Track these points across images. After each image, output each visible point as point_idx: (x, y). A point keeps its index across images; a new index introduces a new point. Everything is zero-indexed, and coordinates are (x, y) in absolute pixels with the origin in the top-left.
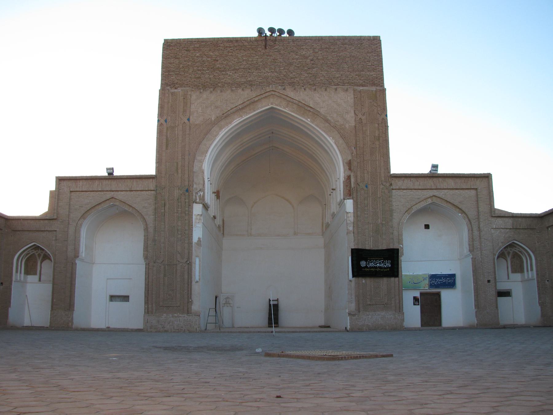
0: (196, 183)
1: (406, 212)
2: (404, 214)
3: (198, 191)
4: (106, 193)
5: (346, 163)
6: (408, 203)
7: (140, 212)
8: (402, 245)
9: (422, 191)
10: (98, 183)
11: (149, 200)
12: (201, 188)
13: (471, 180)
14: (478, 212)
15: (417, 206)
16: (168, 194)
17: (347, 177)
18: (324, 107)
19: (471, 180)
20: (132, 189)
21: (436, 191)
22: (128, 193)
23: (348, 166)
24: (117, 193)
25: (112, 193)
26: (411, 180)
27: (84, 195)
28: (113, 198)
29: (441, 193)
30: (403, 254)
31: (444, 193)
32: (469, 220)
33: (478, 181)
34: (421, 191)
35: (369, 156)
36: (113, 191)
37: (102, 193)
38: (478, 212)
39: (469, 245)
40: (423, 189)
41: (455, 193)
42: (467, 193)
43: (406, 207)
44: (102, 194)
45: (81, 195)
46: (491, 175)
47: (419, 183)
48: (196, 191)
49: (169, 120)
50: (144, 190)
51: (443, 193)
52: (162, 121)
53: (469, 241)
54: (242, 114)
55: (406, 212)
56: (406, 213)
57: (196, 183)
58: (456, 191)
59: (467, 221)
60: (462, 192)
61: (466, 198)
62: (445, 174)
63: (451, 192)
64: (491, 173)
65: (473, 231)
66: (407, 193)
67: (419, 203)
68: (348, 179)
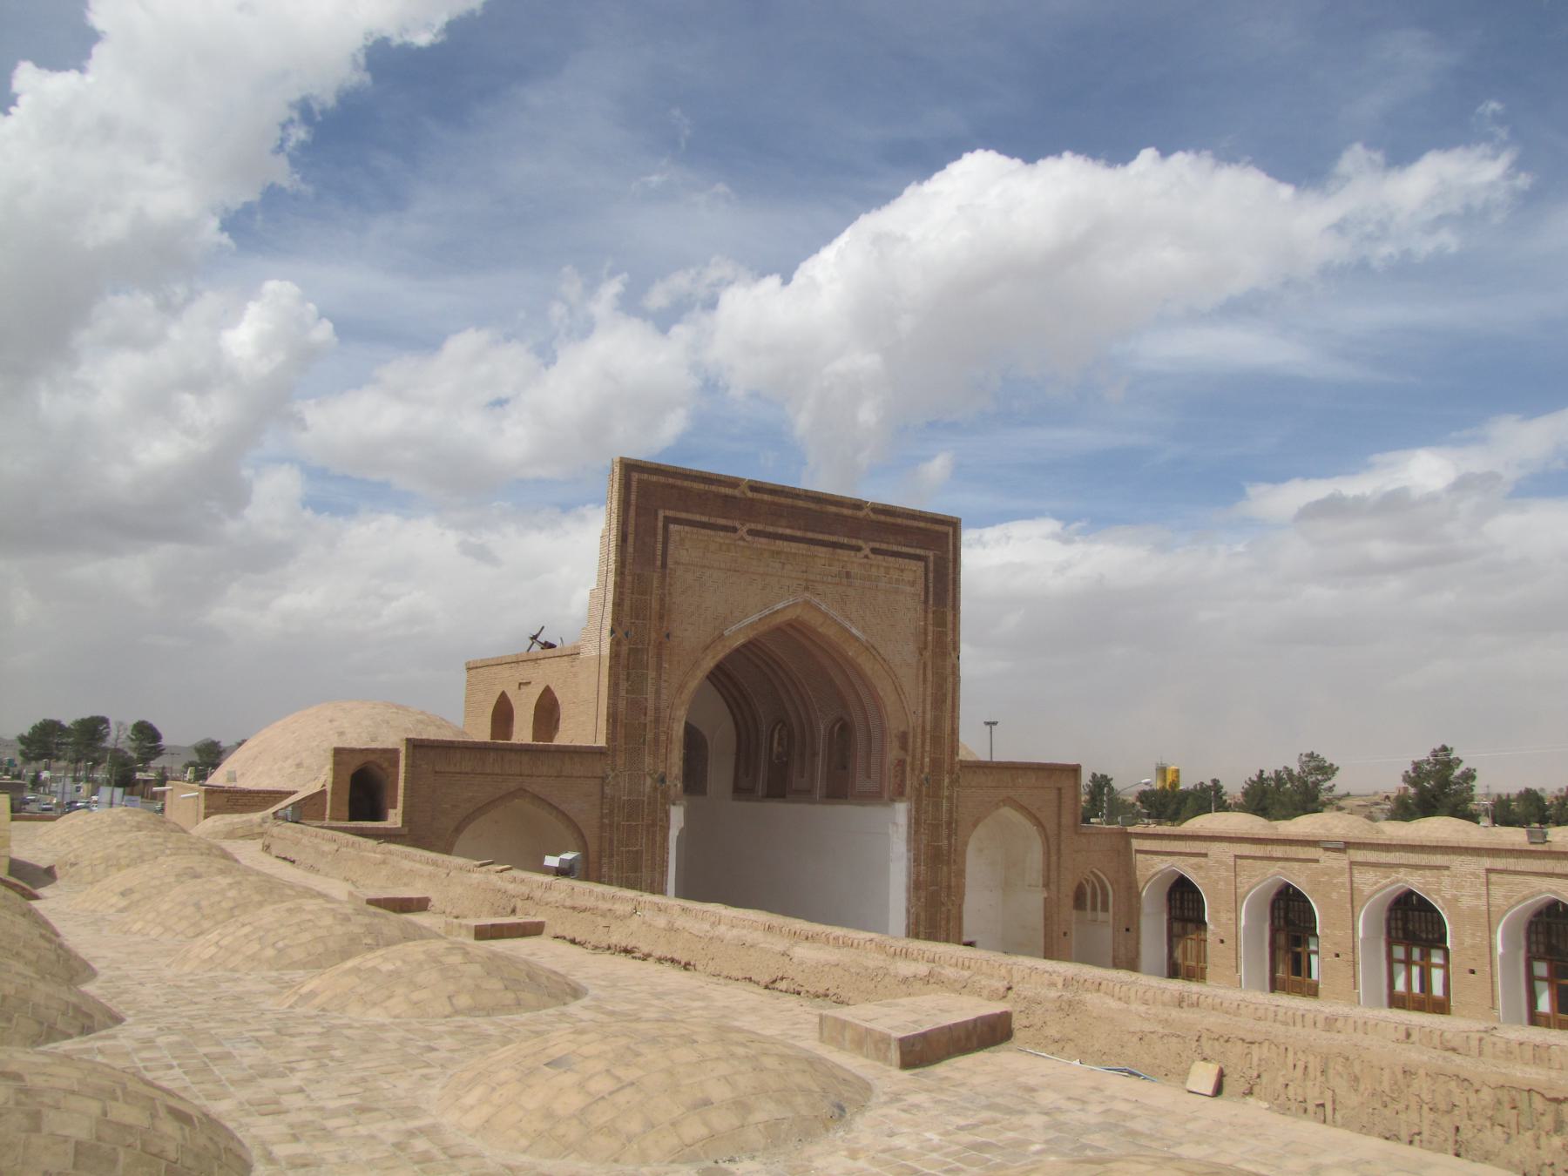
17: (896, 761)
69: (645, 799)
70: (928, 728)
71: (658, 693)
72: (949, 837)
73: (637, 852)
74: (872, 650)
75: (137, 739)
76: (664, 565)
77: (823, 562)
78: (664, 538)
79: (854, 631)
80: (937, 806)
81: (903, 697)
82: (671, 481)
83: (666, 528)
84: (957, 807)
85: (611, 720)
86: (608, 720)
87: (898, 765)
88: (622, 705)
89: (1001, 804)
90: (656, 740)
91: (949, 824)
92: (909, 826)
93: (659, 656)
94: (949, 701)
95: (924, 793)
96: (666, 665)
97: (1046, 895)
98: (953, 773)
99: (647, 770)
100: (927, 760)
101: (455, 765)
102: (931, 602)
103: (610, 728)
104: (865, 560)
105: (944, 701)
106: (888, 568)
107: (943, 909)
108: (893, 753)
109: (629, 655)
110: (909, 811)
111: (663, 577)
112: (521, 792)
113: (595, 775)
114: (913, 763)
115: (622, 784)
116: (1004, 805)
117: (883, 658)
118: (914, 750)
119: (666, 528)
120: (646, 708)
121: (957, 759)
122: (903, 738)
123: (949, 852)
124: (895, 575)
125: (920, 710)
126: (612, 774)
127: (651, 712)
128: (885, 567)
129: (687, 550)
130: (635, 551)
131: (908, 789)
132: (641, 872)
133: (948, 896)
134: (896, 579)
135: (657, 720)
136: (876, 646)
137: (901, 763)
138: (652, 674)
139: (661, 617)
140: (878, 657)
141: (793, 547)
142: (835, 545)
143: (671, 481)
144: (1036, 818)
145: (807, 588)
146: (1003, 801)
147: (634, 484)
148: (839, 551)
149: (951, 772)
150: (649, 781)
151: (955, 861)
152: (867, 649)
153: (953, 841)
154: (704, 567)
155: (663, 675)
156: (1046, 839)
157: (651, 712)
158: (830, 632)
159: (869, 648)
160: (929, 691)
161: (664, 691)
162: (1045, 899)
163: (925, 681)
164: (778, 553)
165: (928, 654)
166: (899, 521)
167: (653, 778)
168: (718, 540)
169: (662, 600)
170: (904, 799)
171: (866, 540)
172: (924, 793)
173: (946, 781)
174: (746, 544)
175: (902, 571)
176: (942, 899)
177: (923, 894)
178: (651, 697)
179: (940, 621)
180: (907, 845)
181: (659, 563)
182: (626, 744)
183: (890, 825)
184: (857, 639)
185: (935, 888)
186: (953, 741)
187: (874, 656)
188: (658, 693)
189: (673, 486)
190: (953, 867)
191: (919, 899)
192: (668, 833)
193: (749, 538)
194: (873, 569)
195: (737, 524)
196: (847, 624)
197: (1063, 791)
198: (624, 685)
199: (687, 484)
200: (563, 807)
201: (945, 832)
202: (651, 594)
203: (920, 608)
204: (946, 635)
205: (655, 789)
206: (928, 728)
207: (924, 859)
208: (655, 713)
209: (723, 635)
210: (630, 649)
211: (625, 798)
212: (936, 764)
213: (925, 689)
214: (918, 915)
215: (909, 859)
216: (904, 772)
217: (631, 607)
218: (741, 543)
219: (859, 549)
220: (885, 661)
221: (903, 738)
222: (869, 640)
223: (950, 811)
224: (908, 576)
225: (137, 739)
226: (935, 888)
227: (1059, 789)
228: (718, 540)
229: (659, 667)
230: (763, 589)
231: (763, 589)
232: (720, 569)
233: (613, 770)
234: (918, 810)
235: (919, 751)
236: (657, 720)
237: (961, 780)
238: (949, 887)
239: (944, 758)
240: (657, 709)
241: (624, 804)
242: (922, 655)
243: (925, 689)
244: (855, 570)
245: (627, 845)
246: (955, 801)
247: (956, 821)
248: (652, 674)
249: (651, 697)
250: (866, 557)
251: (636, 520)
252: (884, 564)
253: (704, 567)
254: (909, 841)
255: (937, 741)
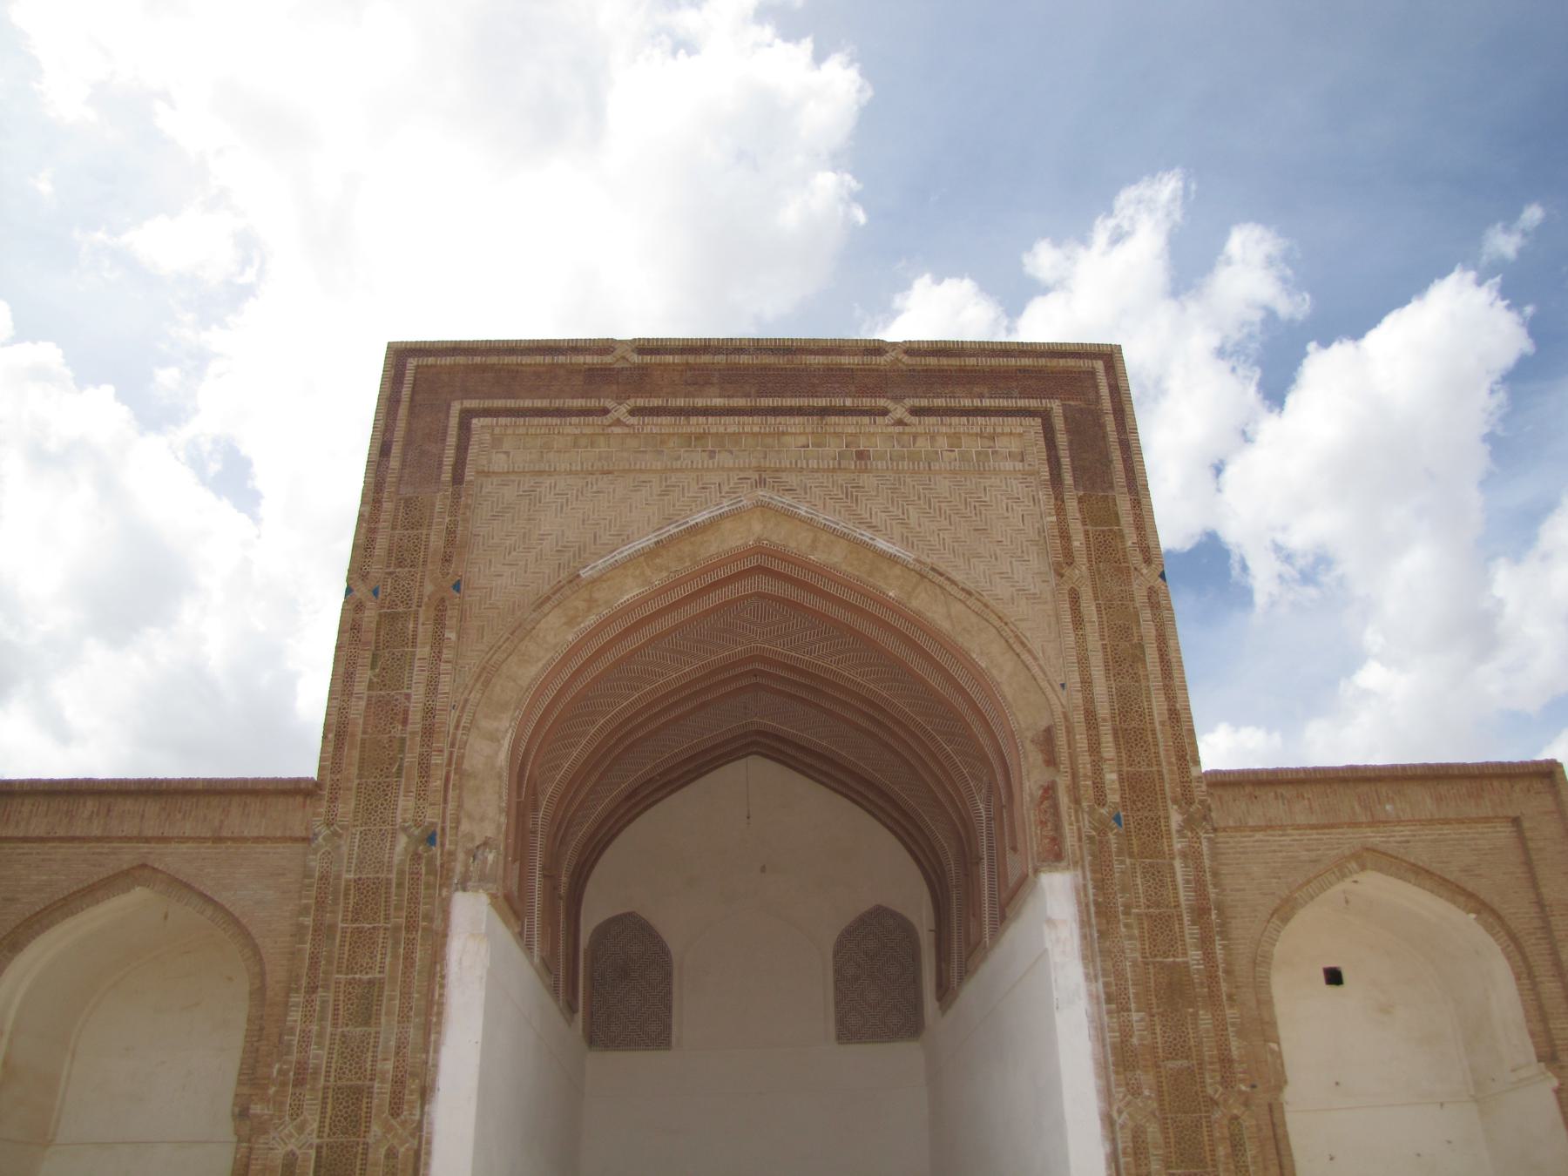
0: (470, 817)
1: (1272, 915)
2: (1268, 922)
3: (477, 843)
4: (124, 848)
5: (1032, 741)
6: (1279, 878)
7: (244, 921)
8: (1274, 1042)
9: (1324, 834)
10: (95, 810)
11: (283, 874)
12: (489, 835)
13: (1491, 784)
14: (1540, 903)
15: (1310, 890)
16: (359, 855)
17: (1040, 792)
18: (972, 532)
19: (1491, 784)
20: (225, 833)
21: (1373, 832)
22: (208, 848)
23: (1042, 751)
24: (161, 845)
25: (144, 848)
26: (1276, 793)
27: (31, 854)
28: (144, 866)
29: (1391, 839)
30: (1286, 1082)
31: (1404, 839)
32: (1513, 938)
33: (1517, 788)
34: (1318, 834)
35: (1117, 711)
36: (147, 840)
37: (106, 848)
38: (1540, 903)
39: (1532, 1034)
40: (1325, 827)
41: (1442, 837)
42: (1483, 833)
43: (1273, 893)
44: (106, 850)
45: (19, 854)
46: (1560, 766)
47: (1306, 802)
48: (470, 846)
49: (389, 591)
50: (268, 838)
51: (1399, 839)
52: (362, 591)
53: (1528, 1021)
54: (650, 574)
55: (1272, 915)
56: (1275, 916)
57: (470, 817)
58: (1442, 829)
59: (1505, 938)
60: (1467, 833)
61: (1486, 854)
62: (1396, 765)
63: (1427, 832)
64: (1559, 760)
65: (1538, 979)
66: (1268, 841)
67: (1315, 878)
68: (1047, 799)
69: (393, 876)
70: (1103, 710)
71: (432, 686)
72: (1205, 942)
73: (371, 982)
74: (931, 575)
75: (1207, 1011)
76: (458, 479)
77: (802, 440)
78: (459, 438)
79: (882, 544)
80: (1158, 875)
81: (1025, 656)
82: (478, 360)
83: (465, 427)
84: (1215, 874)
85: (331, 736)
86: (325, 737)
87: (1043, 798)
88: (358, 708)
89: (1353, 865)
90: (425, 769)
91: (1200, 913)
92: (1084, 923)
93: (439, 622)
94: (1152, 655)
95: (1114, 848)
96: (451, 635)
97: (1555, 1083)
98: (1190, 803)
99: (399, 820)
100: (1111, 777)
101: (17, 826)
102: (1068, 479)
103: (330, 749)
104: (899, 429)
105: (1138, 657)
106: (957, 436)
107: (1217, 1115)
108: (1031, 777)
109: (379, 623)
110: (1080, 891)
111: (456, 497)
112: (139, 873)
113: (288, 834)
114: (1074, 788)
115: (345, 849)
116: (1363, 868)
117: (963, 589)
118: (1073, 758)
119: (465, 427)
120: (406, 712)
121: (1194, 772)
122: (1047, 740)
123: (1212, 978)
124: (973, 446)
125: (1075, 678)
126: (325, 832)
127: (416, 717)
128: (949, 436)
129: (507, 453)
130: (404, 464)
131: (1070, 841)
132: (378, 1024)
133: (1227, 1082)
134: (978, 453)
135: (429, 732)
136: (942, 567)
137: (1049, 791)
138: (423, 651)
139: (447, 559)
140: (949, 587)
141: (731, 424)
142: (824, 412)
143: (478, 360)
144: (1471, 896)
145: (761, 483)
146: (1355, 856)
147: (409, 376)
148: (833, 419)
149: (1185, 799)
150: (403, 840)
151: (1230, 997)
152: (923, 576)
153: (1219, 953)
154: (541, 473)
155: (445, 651)
156: (1514, 944)
157: (416, 717)
158: (833, 556)
159: (927, 575)
160: (1094, 641)
161: (445, 679)
162: (1558, 1091)
163: (1078, 621)
164: (701, 437)
165: (1082, 568)
166: (972, 361)
167: (409, 837)
168: (568, 430)
169: (451, 532)
170: (1064, 864)
171: (897, 399)
172: (1114, 848)
173: (1176, 819)
174: (626, 430)
175: (992, 437)
176: (1210, 1091)
177: (1146, 1079)
178: (418, 694)
179: (1101, 515)
180: (1086, 966)
181: (447, 476)
182: (360, 776)
183: (1045, 928)
184: (893, 560)
185: (1181, 1063)
186: (1177, 737)
187: (940, 587)
188: (432, 686)
189: (484, 368)
190: (1229, 1012)
191: (1135, 1091)
192: (443, 945)
193: (633, 420)
194: (920, 442)
195: (609, 404)
196: (866, 535)
197: (1526, 824)
198: (364, 675)
199: (507, 360)
200: (223, 898)
201: (1190, 932)
202: (430, 526)
203: (1044, 496)
204: (1122, 537)
205: (416, 857)
206: (1103, 710)
207: (1136, 994)
208: (424, 719)
209: (578, 576)
210: (380, 615)
211: (351, 876)
212: (1139, 787)
213: (1081, 640)
214: (1137, 1135)
215: (1094, 998)
216: (1055, 807)
217: (390, 551)
218: (617, 430)
219: (884, 412)
220: (970, 593)
221: (1047, 740)
222: (924, 558)
223: (1199, 887)
224: (1003, 445)
225: (1207, 1011)
226: (1181, 1063)
227: (1516, 821)
228: (568, 430)
229: (438, 640)
230: (664, 493)
231: (664, 493)
232: (570, 472)
233: (329, 824)
234: (1100, 886)
235: (1084, 761)
236: (429, 732)
237: (1213, 814)
238: (1226, 1061)
239: (1160, 773)
240: (429, 712)
241: (347, 890)
242: (1062, 576)
243: (1081, 640)
244: (879, 445)
245: (350, 970)
246: (1207, 863)
247: (1220, 909)
248: (423, 651)
249: (418, 694)
250: (900, 422)
251: (409, 423)
252: (944, 429)
253: (541, 473)
254: (1087, 959)
255: (1132, 735)
